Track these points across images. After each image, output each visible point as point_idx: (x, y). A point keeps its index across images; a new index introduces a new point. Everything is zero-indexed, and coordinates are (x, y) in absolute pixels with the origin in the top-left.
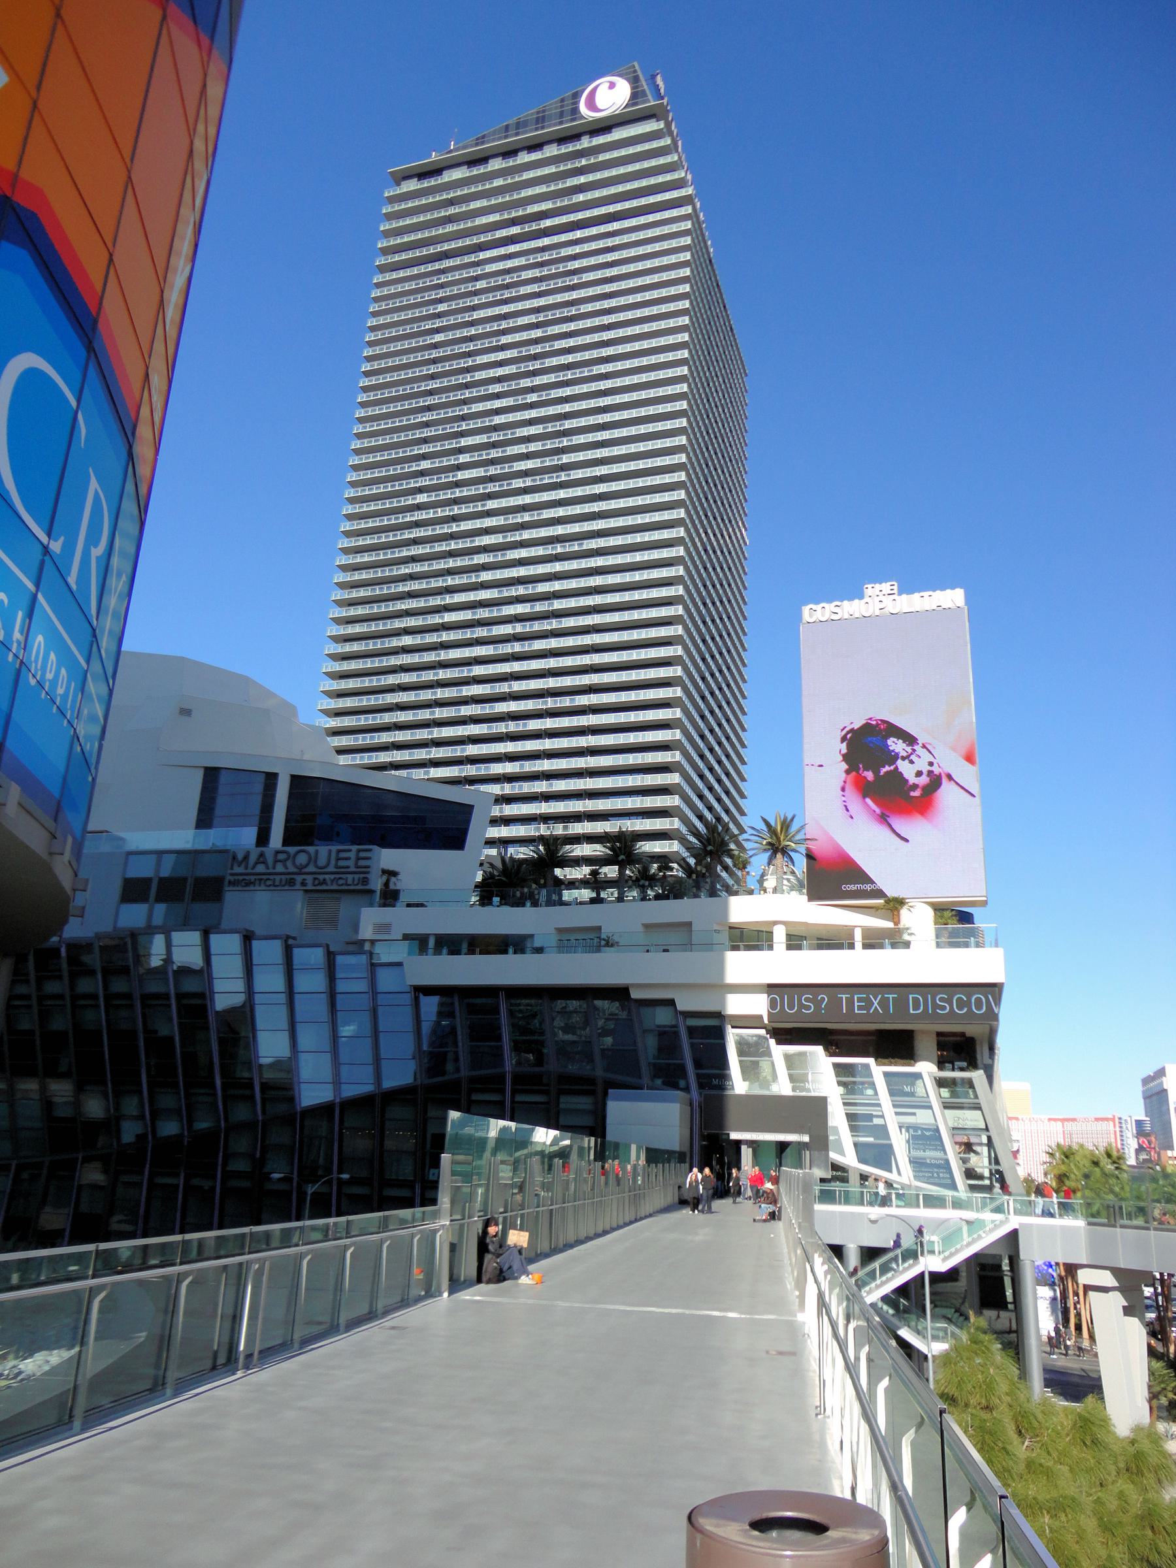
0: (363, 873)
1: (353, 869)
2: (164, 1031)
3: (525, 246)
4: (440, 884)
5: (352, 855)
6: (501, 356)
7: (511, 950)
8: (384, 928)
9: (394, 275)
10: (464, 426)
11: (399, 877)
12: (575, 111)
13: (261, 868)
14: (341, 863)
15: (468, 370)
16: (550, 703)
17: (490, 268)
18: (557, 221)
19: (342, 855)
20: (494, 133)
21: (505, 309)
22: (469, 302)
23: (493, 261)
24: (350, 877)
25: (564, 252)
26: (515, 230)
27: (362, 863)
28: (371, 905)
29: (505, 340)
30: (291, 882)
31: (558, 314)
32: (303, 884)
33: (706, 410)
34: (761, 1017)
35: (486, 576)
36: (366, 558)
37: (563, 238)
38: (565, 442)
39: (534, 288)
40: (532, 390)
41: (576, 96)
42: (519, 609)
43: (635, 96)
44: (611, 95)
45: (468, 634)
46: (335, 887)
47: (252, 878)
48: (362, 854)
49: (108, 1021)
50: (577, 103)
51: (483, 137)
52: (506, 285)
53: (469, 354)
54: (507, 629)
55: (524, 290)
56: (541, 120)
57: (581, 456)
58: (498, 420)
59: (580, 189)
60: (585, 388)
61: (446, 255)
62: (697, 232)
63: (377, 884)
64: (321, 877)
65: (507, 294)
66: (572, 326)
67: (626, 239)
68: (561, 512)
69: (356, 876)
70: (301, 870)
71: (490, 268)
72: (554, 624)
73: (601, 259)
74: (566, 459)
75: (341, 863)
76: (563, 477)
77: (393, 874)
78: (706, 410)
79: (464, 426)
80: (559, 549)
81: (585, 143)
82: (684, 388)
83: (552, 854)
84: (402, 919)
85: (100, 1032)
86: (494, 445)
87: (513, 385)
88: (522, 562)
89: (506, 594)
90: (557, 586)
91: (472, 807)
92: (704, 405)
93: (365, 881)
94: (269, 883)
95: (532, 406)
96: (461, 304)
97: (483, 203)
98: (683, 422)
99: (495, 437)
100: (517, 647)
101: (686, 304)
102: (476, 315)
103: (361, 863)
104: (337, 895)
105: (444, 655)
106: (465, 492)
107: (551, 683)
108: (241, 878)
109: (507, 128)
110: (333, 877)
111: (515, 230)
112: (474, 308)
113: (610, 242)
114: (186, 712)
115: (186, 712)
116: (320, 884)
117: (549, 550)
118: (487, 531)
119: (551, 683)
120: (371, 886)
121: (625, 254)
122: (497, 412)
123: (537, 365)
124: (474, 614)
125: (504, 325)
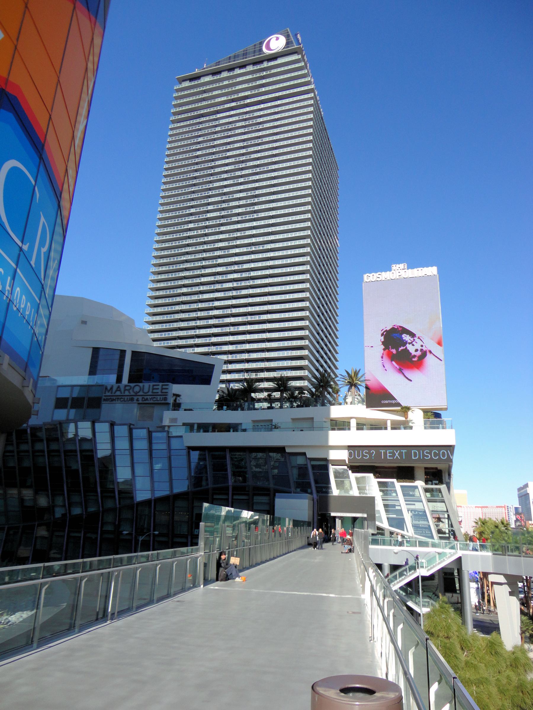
0: (165, 395)
1: (160, 394)
2: (74, 467)
3: (238, 111)
4: (199, 400)
5: (160, 387)
6: (227, 161)
7: (231, 430)
8: (174, 420)
9: (179, 125)
10: (210, 193)
11: (181, 397)
12: (261, 50)
13: (118, 393)
14: (155, 391)
15: (212, 168)
16: (249, 318)
17: (222, 121)
18: (252, 100)
19: (155, 387)
20: (224, 60)
21: (229, 140)
22: (212, 137)
23: (223, 118)
24: (159, 397)
25: (256, 114)
26: (233, 104)
27: (164, 391)
28: (168, 410)
29: (229, 154)
30: (132, 400)
31: (253, 142)
32: (137, 400)
33: (320, 186)
34: (345, 460)
35: (220, 261)
36: (166, 253)
37: (255, 108)
38: (256, 200)
39: (242, 130)
40: (241, 176)
41: (261, 43)
42: (235, 276)
43: (288, 43)
44: (277, 43)
45: (212, 287)
46: (152, 402)
47: (114, 398)
48: (164, 387)
49: (49, 462)
50: (262, 47)
51: (219, 62)
52: (229, 129)
53: (213, 160)
54: (230, 285)
55: (237, 131)
56: (245, 54)
57: (263, 207)
58: (226, 190)
60: (265, 176)
61: (202, 116)
62: (316, 105)
63: (171, 400)
64: (146, 397)
65: (230, 133)
66: (259, 148)
67: (284, 108)
68: (254, 232)
69: (162, 397)
70: (136, 394)
71: (222, 121)
72: (251, 283)
73: (273, 117)
74: (256, 208)
75: (155, 391)
76: (255, 216)
77: (178, 396)
78: (320, 186)
79: (210, 193)
80: (253, 249)
81: (265, 65)
82: (310, 175)
83: (250, 387)
84: (182, 416)
85: (45, 467)
86: (224, 202)
87: (233, 174)
88: (236, 255)
89: (229, 269)
90: (252, 265)
91: (214, 365)
92: (319, 184)
93: (166, 399)
94: (122, 400)
95: (241, 184)
97: (219, 92)
98: (310, 191)
99: (224, 198)
100: (234, 293)
101: (311, 138)
102: (216, 143)
103: (164, 391)
104: (153, 405)
105: (201, 297)
106: (211, 223)
107: (250, 309)
108: (109, 397)
109: (230, 58)
110: (151, 397)
111: (233, 104)
112: (215, 140)
113: (276, 110)
114: (84, 322)
115: (84, 322)
116: (145, 400)
117: (249, 249)
118: (221, 241)
119: (250, 309)
120: (168, 401)
121: (283, 115)
122: (225, 186)
123: (243, 165)
124: (215, 278)
125: (228, 147)
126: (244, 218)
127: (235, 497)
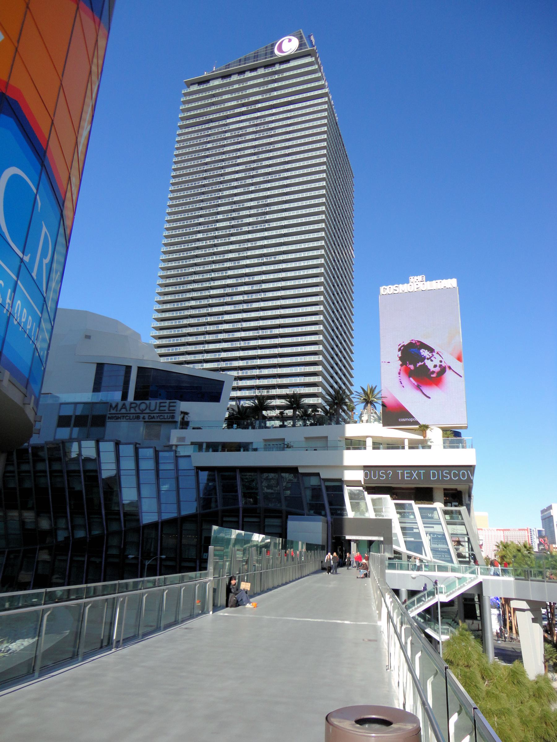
0: (172, 413)
1: (167, 411)
3: (249, 116)
4: (208, 418)
5: (167, 404)
6: (237, 168)
7: (242, 450)
8: (182, 439)
9: (187, 130)
10: (220, 202)
11: (189, 415)
12: (272, 52)
13: (123, 411)
14: (162, 408)
15: (222, 175)
17: (232, 127)
18: (264, 104)
19: (162, 405)
20: (234, 63)
21: (239, 146)
22: (222, 143)
23: (233, 124)
24: (166, 415)
25: (267, 119)
26: (244, 109)
27: (171, 408)
28: (176, 428)
29: (239, 161)
30: (138, 418)
31: (264, 148)
32: (144, 418)
33: (334, 194)
35: (230, 273)
36: (173, 264)
37: (267, 112)
38: (268, 209)
39: (253, 136)
40: (252, 184)
41: (273, 45)
42: (246, 288)
43: (301, 45)
44: (289, 45)
45: (222, 300)
46: (159, 420)
48: (172, 404)
49: (51, 483)
50: (273, 49)
51: (229, 65)
52: (240, 135)
53: (222, 168)
54: (240, 298)
55: (248, 137)
56: (256, 57)
57: (275, 216)
58: (236, 199)
59: (275, 89)
60: (277, 184)
61: (211, 121)
62: (330, 110)
63: (179, 418)
64: (152, 415)
65: (240, 139)
66: (271, 154)
67: (296, 113)
68: (266, 242)
69: (169, 415)
70: (142, 412)
71: (232, 127)
73: (285, 123)
74: (268, 217)
75: (162, 408)
76: (267, 226)
77: (186, 413)
78: (334, 194)
79: (220, 202)
80: (265, 260)
81: (277, 68)
82: (324, 183)
83: (261, 404)
84: (190, 435)
85: (47, 488)
86: (234, 211)
87: (243, 182)
88: (247, 266)
89: (240, 281)
90: (264, 277)
91: (224, 382)
92: (333, 192)
93: (173, 417)
94: (127, 418)
95: (252, 192)
96: (219, 144)
97: (229, 96)
98: (324, 200)
99: (234, 207)
100: (245, 306)
101: (325, 144)
102: (226, 149)
103: (171, 408)
104: (160, 424)
105: (210, 310)
106: (220, 233)
107: (261, 323)
108: (114, 415)
109: (240, 60)
110: (157, 415)
111: (244, 109)
112: (224, 146)
113: (289, 115)
114: (88, 337)
115: (88, 337)
116: (152, 418)
117: (260, 260)
118: (231, 251)
119: (261, 323)
121: (296, 120)
122: (236, 195)
123: (254, 173)
124: (224, 290)
125: (239, 154)
126: (255, 227)
127: (246, 520)
